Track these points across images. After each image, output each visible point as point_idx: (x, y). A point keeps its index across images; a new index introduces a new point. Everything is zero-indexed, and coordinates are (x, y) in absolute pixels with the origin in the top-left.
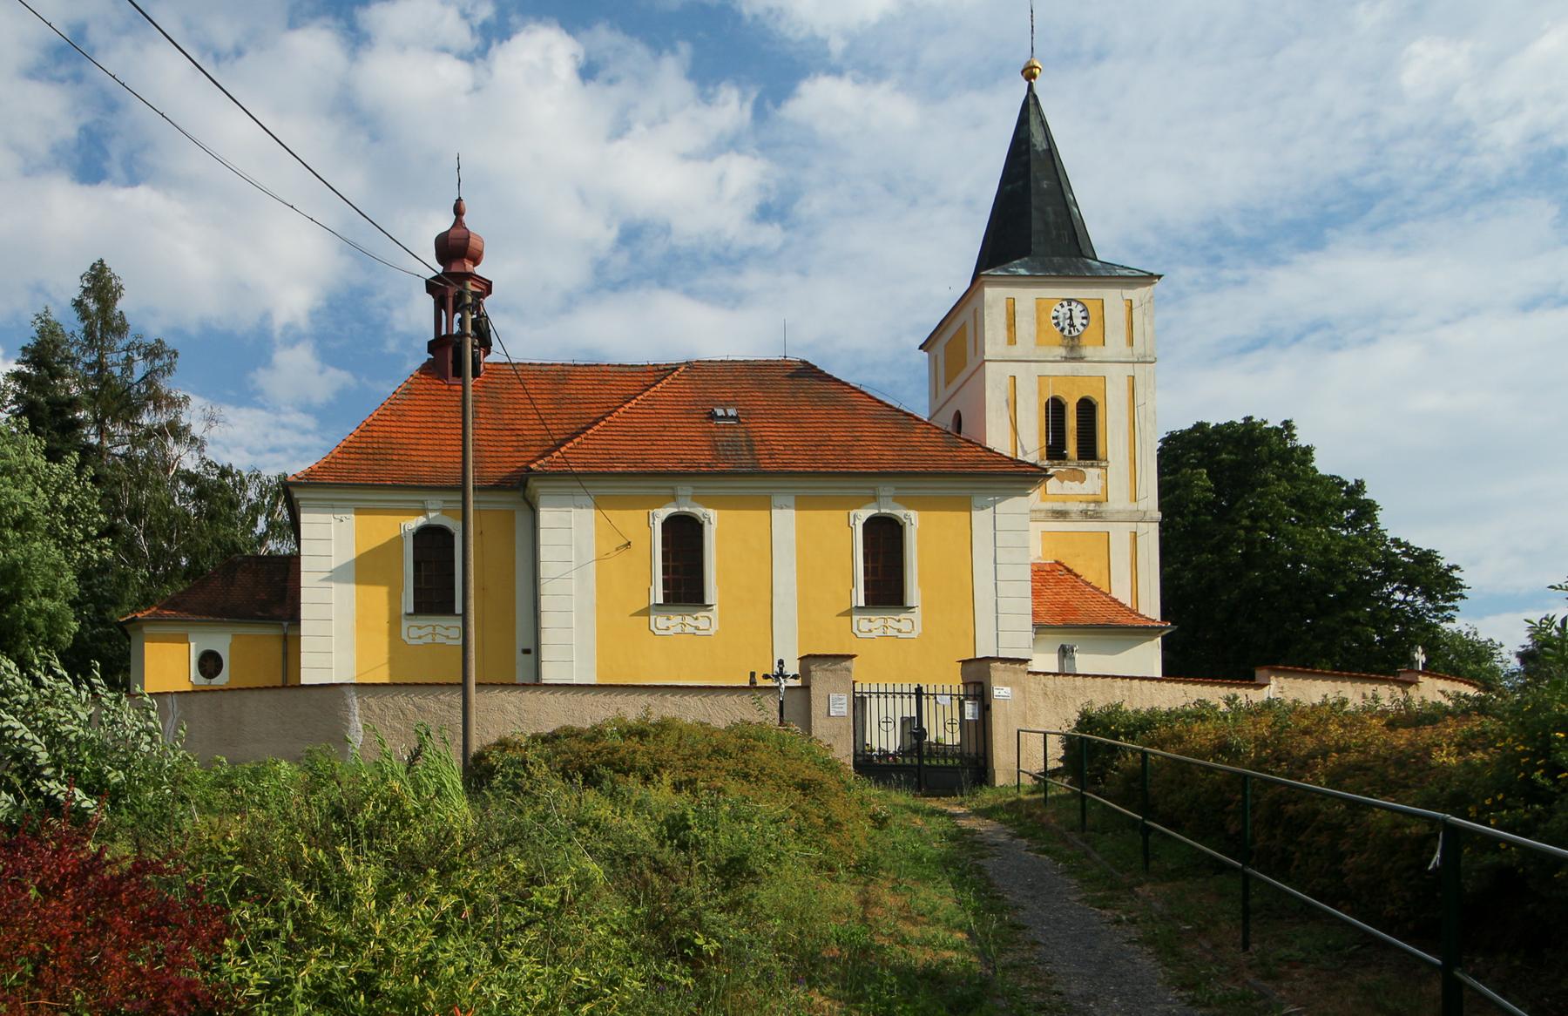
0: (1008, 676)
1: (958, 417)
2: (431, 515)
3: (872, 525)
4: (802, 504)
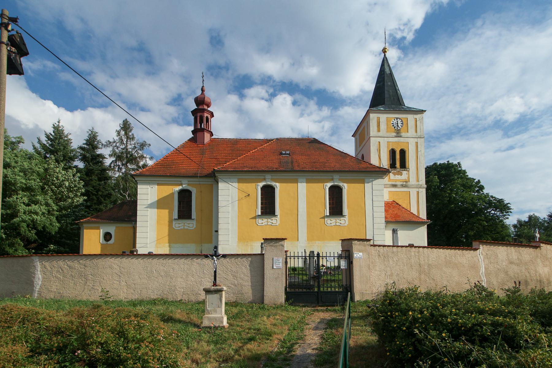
0: (362, 247)
1: (363, 156)
2: (184, 186)
3: (332, 188)
4: (308, 181)
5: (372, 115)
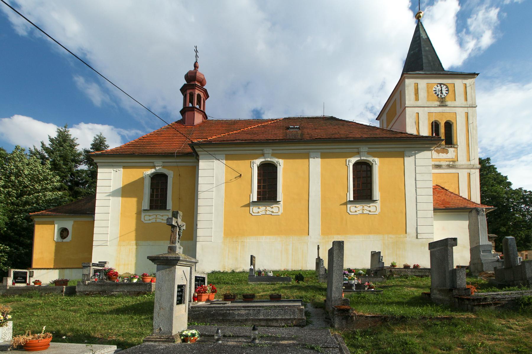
2: (157, 168)
4: (323, 156)
5: (408, 81)
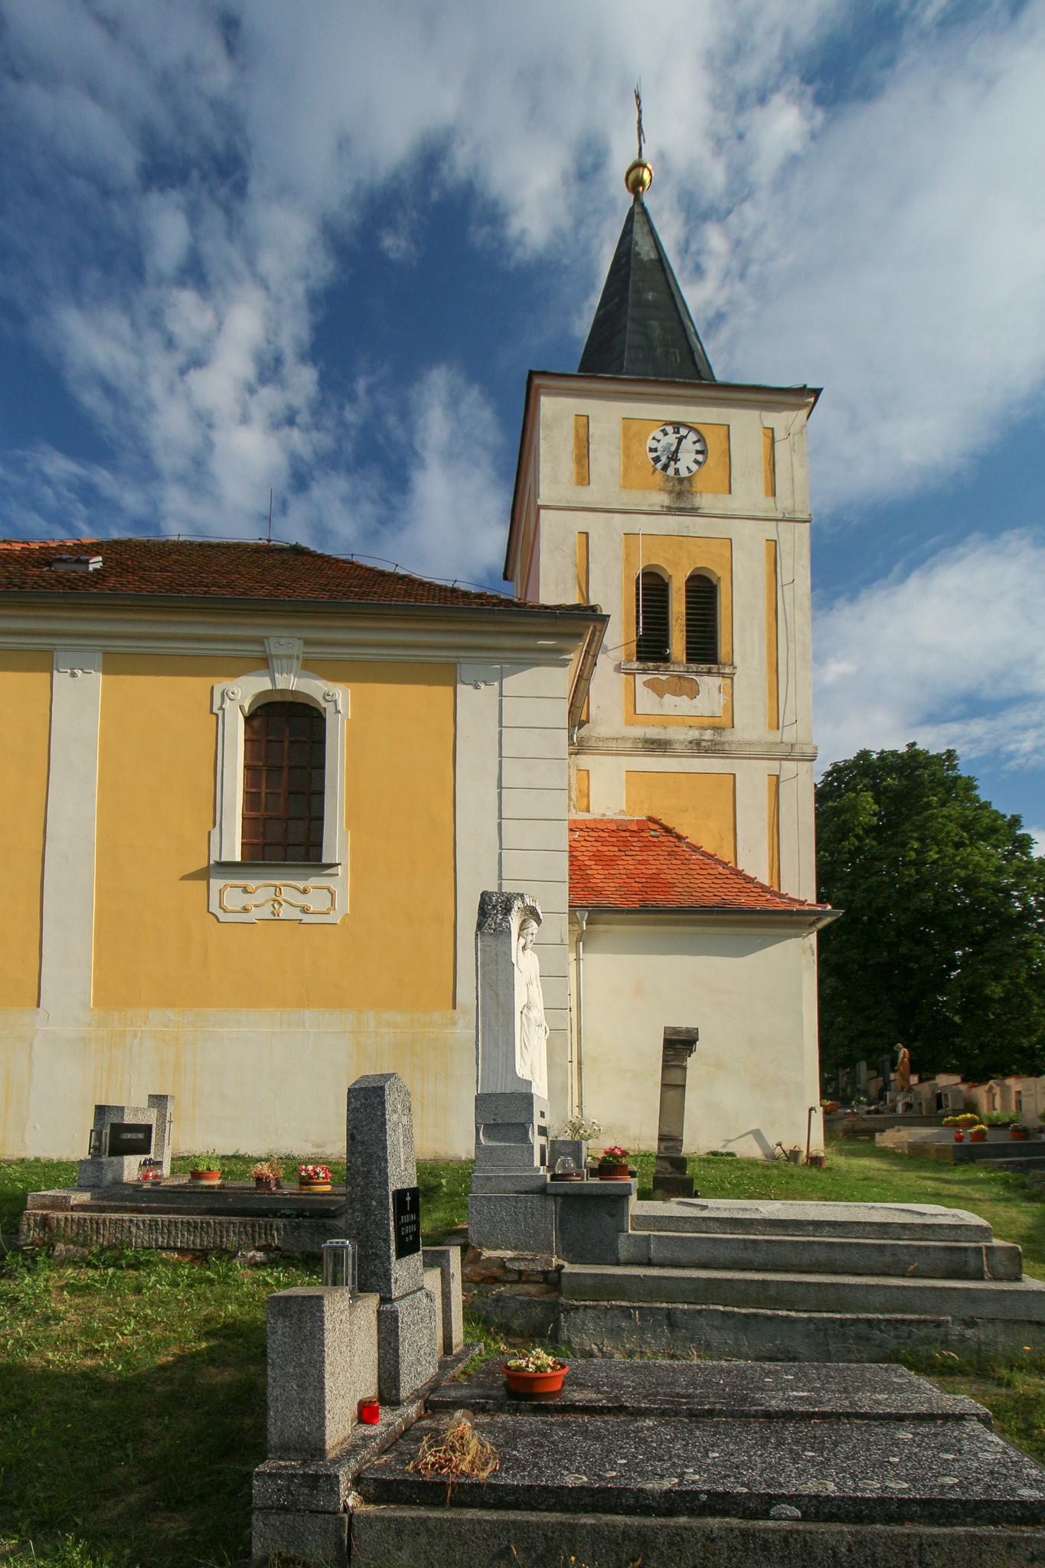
4: (113, 665)
